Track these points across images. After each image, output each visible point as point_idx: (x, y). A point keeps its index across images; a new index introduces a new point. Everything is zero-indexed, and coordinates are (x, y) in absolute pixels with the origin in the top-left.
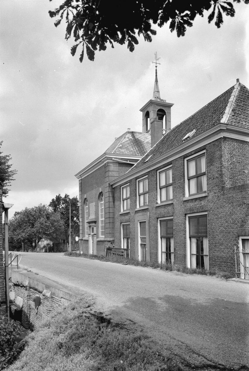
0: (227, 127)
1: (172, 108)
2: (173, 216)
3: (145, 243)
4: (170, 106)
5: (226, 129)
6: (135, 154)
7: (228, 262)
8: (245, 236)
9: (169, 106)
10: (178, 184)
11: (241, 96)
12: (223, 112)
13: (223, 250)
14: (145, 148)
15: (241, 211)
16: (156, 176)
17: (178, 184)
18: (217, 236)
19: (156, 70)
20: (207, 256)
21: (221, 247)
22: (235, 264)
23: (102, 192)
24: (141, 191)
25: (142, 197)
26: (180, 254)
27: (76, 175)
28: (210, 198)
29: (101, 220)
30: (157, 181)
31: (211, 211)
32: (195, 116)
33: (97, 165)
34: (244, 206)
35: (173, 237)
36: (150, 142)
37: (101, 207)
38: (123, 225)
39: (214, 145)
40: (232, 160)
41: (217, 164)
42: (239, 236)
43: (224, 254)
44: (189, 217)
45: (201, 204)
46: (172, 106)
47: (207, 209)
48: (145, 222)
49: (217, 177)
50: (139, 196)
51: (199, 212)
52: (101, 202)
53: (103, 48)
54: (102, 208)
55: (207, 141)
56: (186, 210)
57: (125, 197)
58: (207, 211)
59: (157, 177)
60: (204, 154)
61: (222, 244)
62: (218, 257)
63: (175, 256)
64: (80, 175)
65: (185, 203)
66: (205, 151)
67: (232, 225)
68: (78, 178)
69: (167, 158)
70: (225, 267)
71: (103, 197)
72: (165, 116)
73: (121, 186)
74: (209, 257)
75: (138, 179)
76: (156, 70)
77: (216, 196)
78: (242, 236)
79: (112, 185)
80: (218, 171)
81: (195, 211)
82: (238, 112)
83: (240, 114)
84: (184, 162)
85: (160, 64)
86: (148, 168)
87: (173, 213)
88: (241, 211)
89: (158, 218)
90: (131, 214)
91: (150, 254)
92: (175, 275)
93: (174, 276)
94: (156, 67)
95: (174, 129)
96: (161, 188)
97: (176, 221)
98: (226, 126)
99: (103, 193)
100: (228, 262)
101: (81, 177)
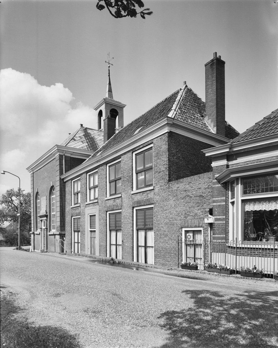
0: (174, 122)
1: (124, 109)
2: (121, 209)
3: (94, 236)
4: (123, 107)
5: (172, 123)
6: (88, 149)
7: (171, 253)
8: (188, 227)
9: (122, 107)
10: (126, 177)
11: (187, 97)
12: (170, 109)
13: (167, 241)
14: (98, 145)
15: (184, 203)
16: (105, 170)
17: (126, 177)
18: (162, 228)
19: (109, 70)
20: (153, 247)
21: (165, 238)
22: (208, 233)
23: (53, 186)
24: (92, 185)
25: (92, 191)
26: (128, 247)
27: (27, 169)
28: (156, 190)
29: (53, 214)
30: (106, 175)
31: (157, 204)
32: (145, 115)
33: (50, 157)
34: (187, 198)
35: (121, 230)
36: (103, 139)
37: (53, 201)
38: (74, 218)
39: (161, 139)
40: (177, 155)
41: (163, 158)
42: (182, 228)
43: (168, 245)
44: (136, 210)
45: (148, 197)
46: (124, 107)
47: (153, 202)
48: (95, 215)
49: (163, 171)
50: (90, 189)
51: (146, 205)
52: (53, 196)
53: (191, 298)
54: (54, 202)
55: (156, 134)
56: (134, 203)
57: (76, 191)
58: (153, 204)
59: (106, 170)
60: (151, 149)
61: (166, 236)
62: (162, 248)
63: (122, 248)
64: (32, 169)
65: (133, 195)
66: (152, 145)
67: (176, 217)
68: (30, 172)
69: (116, 152)
70: (168, 257)
71: (55, 191)
72: (118, 116)
73: (72, 179)
74: (155, 249)
75: (89, 172)
76: (109, 70)
77: (161, 189)
78: (185, 227)
79: (63, 179)
80: (164, 164)
81: (142, 204)
82: (184, 111)
83: (186, 113)
84: (132, 156)
85: (112, 65)
86: (97, 162)
87: (121, 206)
88: (184, 203)
89: (107, 212)
90: (81, 207)
91: (100, 246)
92: (9, 286)
93: (10, 285)
94: (109, 67)
95: (126, 127)
96: (110, 182)
97: (123, 214)
98: (173, 120)
99: (54, 187)
100: (171, 253)
101: (33, 171)
